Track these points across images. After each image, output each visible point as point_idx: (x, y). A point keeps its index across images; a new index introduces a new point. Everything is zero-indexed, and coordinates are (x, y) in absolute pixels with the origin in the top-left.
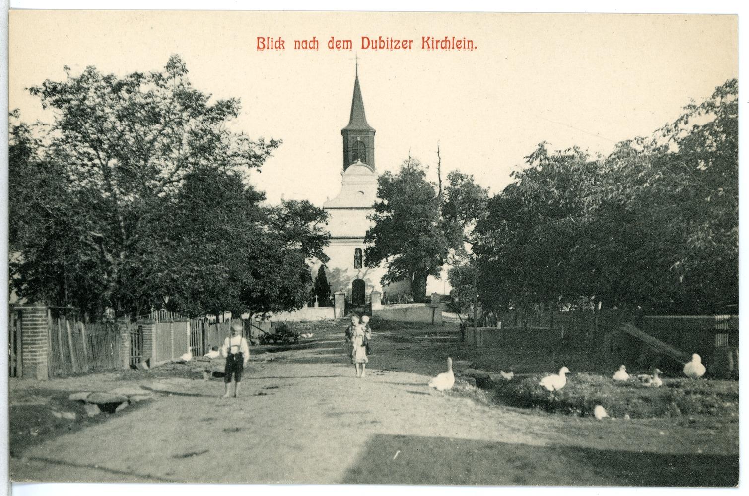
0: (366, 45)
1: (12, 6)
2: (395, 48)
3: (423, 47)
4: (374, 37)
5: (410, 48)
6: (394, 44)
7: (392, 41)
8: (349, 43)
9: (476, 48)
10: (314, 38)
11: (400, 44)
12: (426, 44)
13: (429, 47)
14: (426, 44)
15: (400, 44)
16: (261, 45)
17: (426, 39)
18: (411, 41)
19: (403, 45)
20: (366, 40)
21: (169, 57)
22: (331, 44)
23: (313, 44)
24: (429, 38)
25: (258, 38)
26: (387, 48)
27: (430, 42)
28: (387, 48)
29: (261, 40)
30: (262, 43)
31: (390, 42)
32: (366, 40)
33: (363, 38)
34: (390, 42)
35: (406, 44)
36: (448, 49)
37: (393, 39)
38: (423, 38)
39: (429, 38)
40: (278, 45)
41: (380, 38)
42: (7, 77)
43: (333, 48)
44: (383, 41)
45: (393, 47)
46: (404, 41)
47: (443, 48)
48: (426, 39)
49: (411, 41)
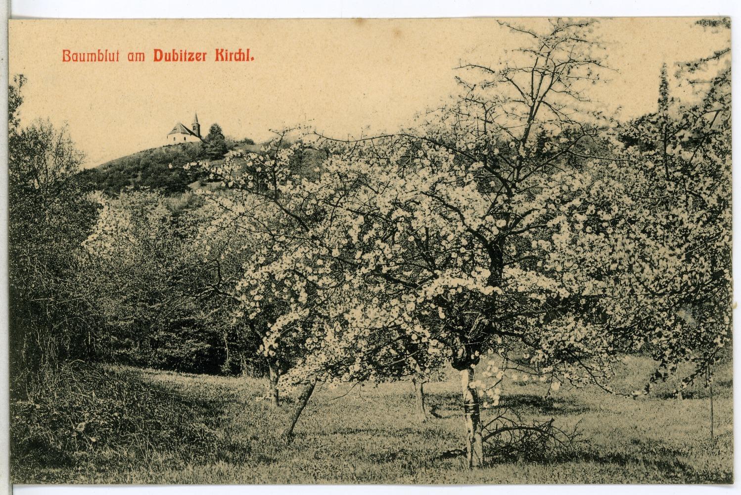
0: (158, 57)
1: (16, 12)
2: (190, 60)
3: (217, 59)
4: (167, 50)
5: (204, 59)
6: (188, 57)
7: (185, 54)
8: (142, 55)
9: (252, 59)
10: (240, 50)
11: (194, 56)
12: (220, 57)
13: (222, 59)
14: (220, 57)
15: (194, 56)
16: (67, 58)
17: (220, 51)
18: (204, 54)
19: (197, 58)
20: (158, 53)
21: (724, 13)
22: (131, 56)
23: (141, 57)
24: (222, 50)
25: (64, 51)
26: (106, 60)
27: (224, 54)
28: (106, 60)
29: (67, 53)
30: (68, 55)
31: (183, 55)
32: (158, 53)
33: (156, 51)
34: (183, 55)
35: (199, 57)
36: (670, 62)
37: (187, 53)
38: (217, 50)
39: (222, 50)
40: (238, 56)
41: (99, 50)
42: (6, 33)
43: (77, 60)
44: (177, 54)
45: (187, 59)
46: (197, 54)
47: (236, 60)
48: (220, 51)
49: (204, 54)
